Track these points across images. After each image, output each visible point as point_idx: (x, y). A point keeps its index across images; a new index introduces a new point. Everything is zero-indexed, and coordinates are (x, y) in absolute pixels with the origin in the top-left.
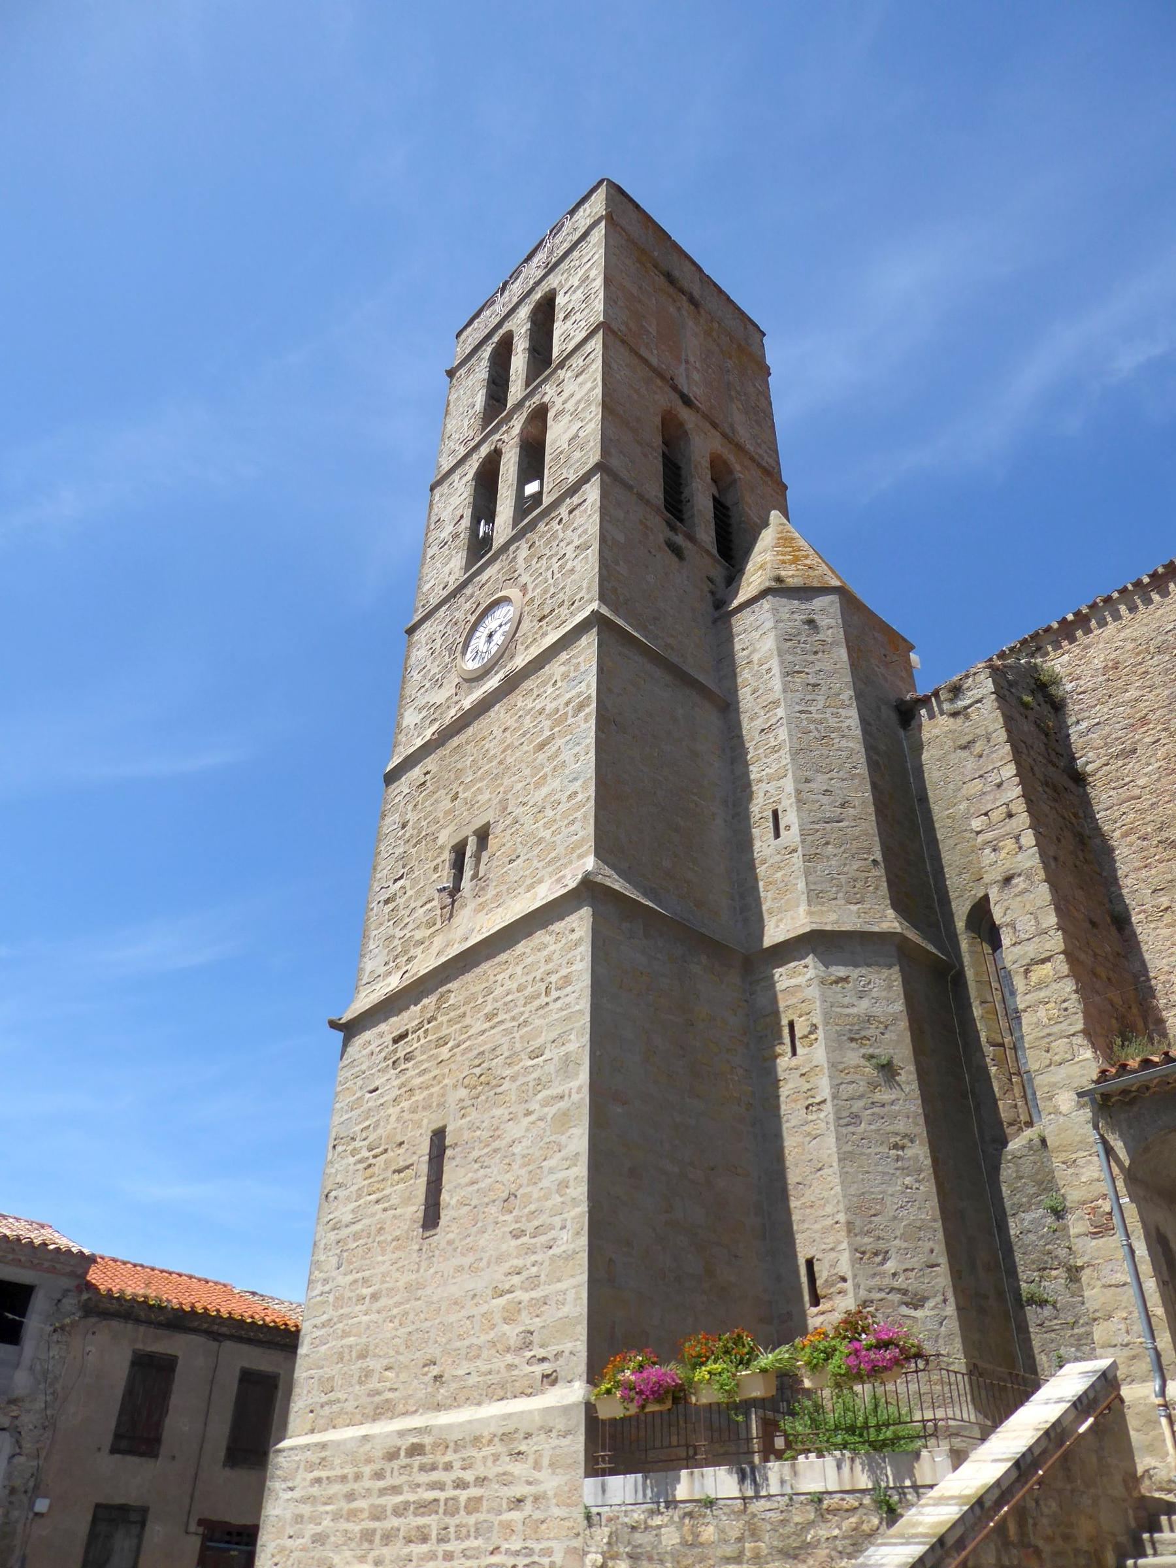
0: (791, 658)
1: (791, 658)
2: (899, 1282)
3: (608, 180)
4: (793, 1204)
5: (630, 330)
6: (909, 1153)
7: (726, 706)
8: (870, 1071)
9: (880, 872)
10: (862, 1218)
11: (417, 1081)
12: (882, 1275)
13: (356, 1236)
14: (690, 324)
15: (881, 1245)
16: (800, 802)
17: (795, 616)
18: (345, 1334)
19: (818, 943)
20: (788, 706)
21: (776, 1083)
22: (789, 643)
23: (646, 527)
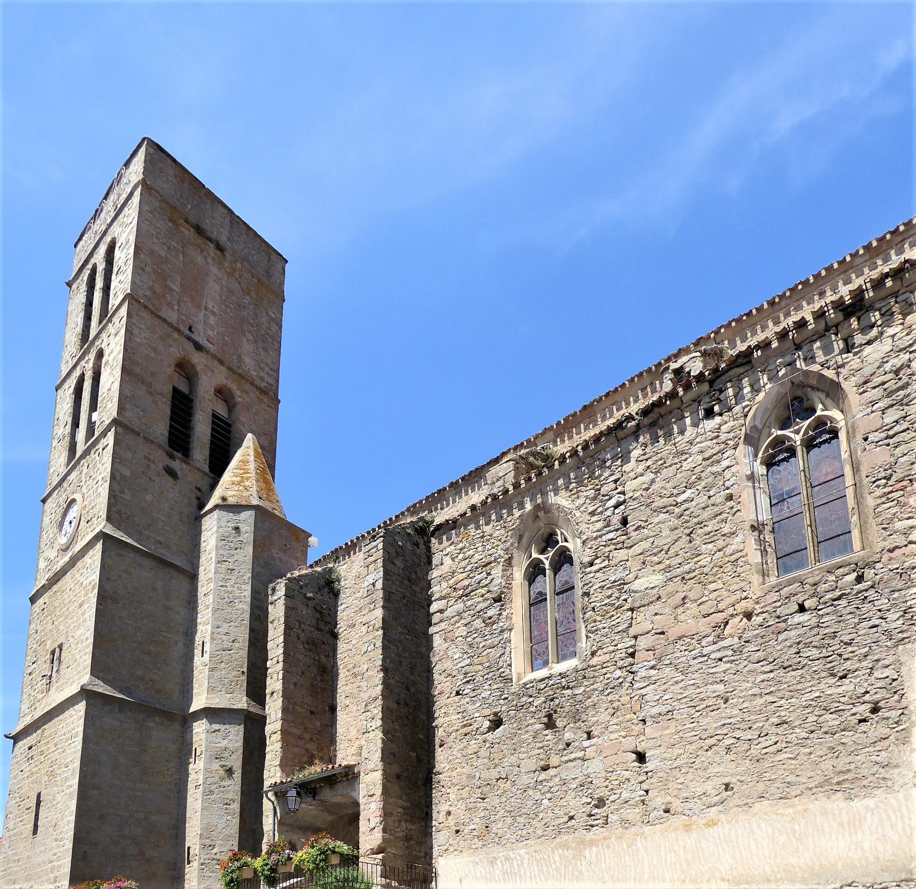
0: (222, 552)
1: (222, 552)
2: (217, 857)
3: (149, 139)
4: (187, 825)
5: (154, 293)
6: (232, 806)
7: (193, 577)
8: (222, 772)
9: (244, 678)
10: (207, 832)
11: (34, 769)
12: (211, 854)
13: (14, 835)
14: (214, 270)
15: (213, 843)
16: (213, 639)
17: (229, 524)
18: (10, 875)
19: (211, 714)
20: (216, 582)
21: (188, 775)
22: (223, 542)
23: (149, 460)
